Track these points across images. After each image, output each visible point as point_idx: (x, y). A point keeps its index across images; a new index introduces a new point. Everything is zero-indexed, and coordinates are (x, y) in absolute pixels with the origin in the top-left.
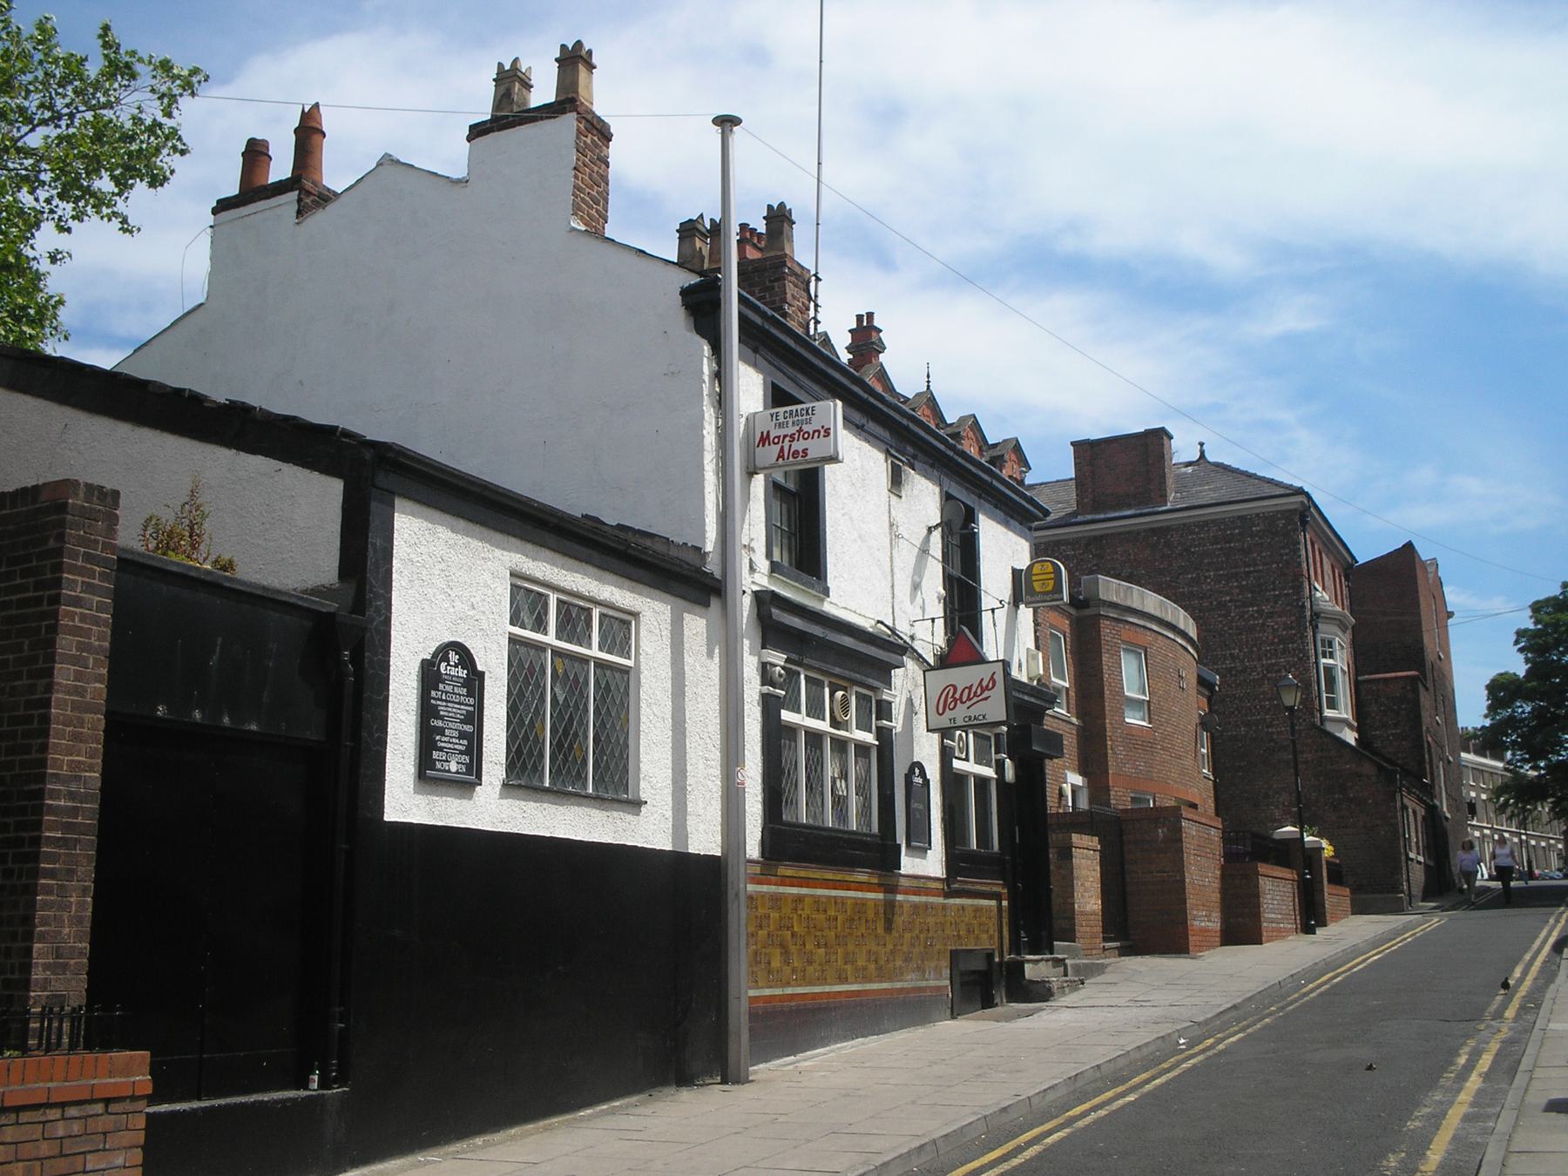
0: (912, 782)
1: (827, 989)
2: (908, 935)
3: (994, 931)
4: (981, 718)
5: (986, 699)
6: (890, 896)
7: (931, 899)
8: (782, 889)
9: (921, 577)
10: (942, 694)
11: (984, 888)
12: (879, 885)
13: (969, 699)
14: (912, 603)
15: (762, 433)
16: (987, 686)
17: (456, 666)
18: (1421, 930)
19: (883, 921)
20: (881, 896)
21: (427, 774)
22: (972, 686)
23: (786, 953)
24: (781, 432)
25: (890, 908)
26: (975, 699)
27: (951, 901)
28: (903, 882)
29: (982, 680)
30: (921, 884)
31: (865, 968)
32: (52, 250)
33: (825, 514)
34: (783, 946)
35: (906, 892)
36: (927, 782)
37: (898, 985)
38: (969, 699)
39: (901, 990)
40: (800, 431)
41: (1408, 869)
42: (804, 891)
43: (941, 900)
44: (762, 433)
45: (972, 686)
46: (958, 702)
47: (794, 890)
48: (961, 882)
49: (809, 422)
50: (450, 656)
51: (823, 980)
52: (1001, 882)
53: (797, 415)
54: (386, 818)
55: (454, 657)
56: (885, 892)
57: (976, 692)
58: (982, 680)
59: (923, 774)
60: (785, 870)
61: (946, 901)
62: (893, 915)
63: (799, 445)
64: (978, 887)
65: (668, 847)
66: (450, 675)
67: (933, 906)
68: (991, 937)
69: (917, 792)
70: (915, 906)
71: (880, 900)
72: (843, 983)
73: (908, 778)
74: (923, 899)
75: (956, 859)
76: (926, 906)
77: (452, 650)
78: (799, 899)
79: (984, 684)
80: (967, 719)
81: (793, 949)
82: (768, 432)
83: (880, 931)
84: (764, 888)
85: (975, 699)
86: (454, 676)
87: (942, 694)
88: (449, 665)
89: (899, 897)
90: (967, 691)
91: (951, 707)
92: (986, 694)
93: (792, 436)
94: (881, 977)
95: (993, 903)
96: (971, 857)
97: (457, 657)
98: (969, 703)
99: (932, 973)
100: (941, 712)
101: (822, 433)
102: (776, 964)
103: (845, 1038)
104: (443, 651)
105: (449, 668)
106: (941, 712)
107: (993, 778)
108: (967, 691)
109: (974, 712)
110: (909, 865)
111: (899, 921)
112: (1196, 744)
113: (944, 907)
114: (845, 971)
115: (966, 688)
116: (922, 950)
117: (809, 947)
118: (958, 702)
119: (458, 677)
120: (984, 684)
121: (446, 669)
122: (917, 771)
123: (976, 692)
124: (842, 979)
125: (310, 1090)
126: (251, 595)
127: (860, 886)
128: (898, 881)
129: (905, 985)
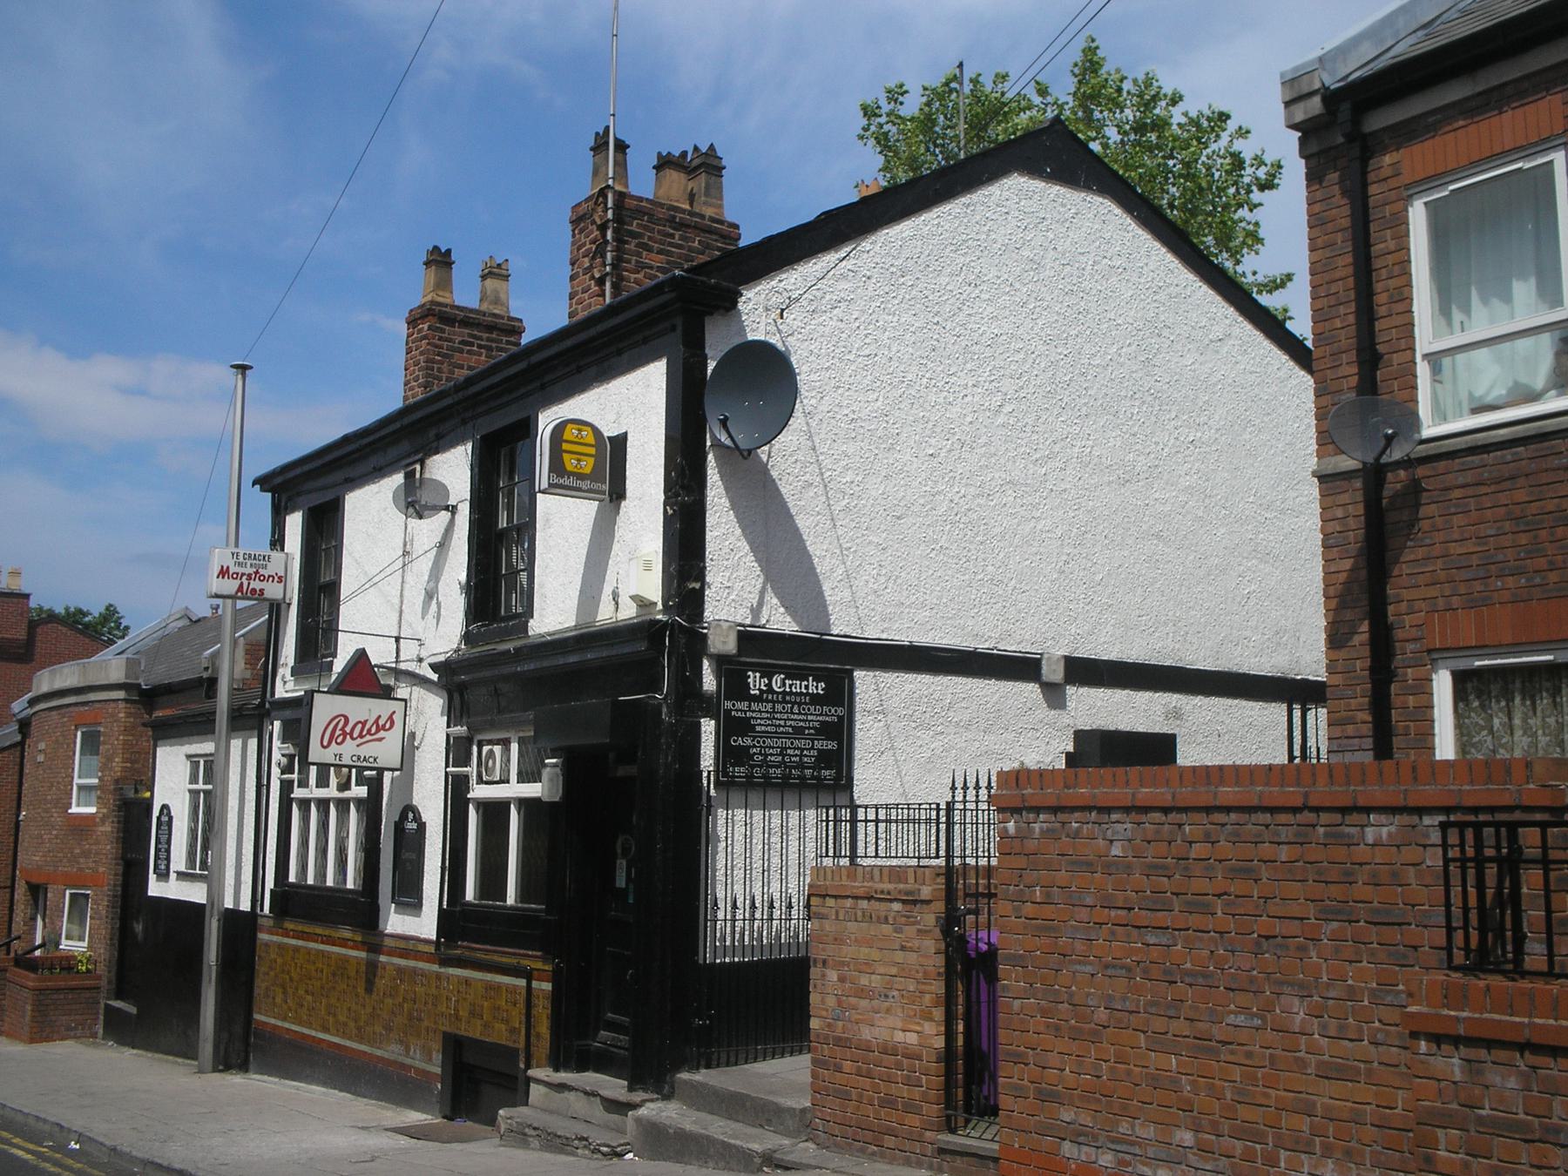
0: (404, 829)
1: (313, 1033)
2: (389, 1001)
3: (520, 1023)
5: (381, 739)
6: (372, 956)
7: (421, 965)
8: (286, 940)
9: (437, 582)
11: (504, 960)
12: (363, 943)
13: (361, 736)
14: (423, 618)
15: (222, 567)
16: (384, 725)
19: (364, 980)
20: (363, 954)
22: (366, 721)
23: (285, 993)
24: (240, 570)
25: (372, 968)
27: (451, 971)
28: (388, 942)
29: (380, 716)
30: (408, 947)
31: (345, 1024)
32: (892, 85)
34: (284, 987)
35: (391, 953)
36: (422, 827)
37: (379, 1053)
38: (361, 736)
39: (381, 1059)
40: (257, 573)
41: (1448, 905)
42: (300, 943)
43: (435, 968)
44: (222, 567)
45: (366, 721)
47: (294, 942)
48: (461, 949)
49: (265, 567)
51: (309, 1025)
52: (539, 954)
53: (255, 559)
54: (150, 893)
56: (368, 951)
57: (369, 730)
58: (380, 716)
59: (417, 818)
60: (289, 925)
61: (442, 970)
62: (375, 976)
63: (256, 585)
64: (496, 958)
65: (231, 907)
67: (423, 974)
68: (513, 1031)
69: (410, 840)
70: (400, 971)
71: (362, 959)
72: (325, 1032)
73: (399, 828)
74: (412, 963)
75: (454, 919)
76: (414, 971)
78: (296, 949)
80: (354, 758)
81: (290, 991)
82: (228, 568)
83: (361, 990)
84: (275, 938)
85: (368, 738)
86: (801, 694)
89: (383, 958)
91: (339, 741)
92: (382, 734)
93: (249, 575)
94: (361, 1040)
95: (522, 982)
96: (470, 912)
98: (359, 741)
99: (418, 1052)
100: (325, 743)
101: (276, 578)
102: (278, 1000)
103: (324, 1084)
106: (325, 743)
108: (360, 726)
109: (365, 751)
110: (396, 923)
111: (381, 983)
112: (1463, 486)
113: (438, 976)
114: (328, 1020)
115: (360, 722)
116: (406, 1022)
117: (301, 992)
120: (381, 722)
121: (784, 685)
122: (411, 815)
123: (369, 730)
124: (326, 1030)
126: (1513, 406)
127: (343, 943)
128: (382, 941)
129: (386, 1055)
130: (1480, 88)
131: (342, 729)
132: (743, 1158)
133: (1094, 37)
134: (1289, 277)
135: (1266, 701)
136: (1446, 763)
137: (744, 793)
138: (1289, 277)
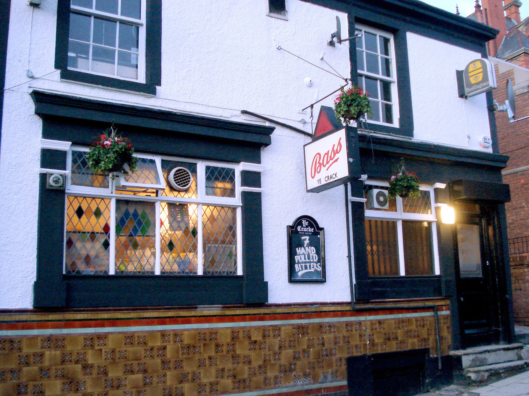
4: (334, 176)
5: (336, 160)
10: (312, 167)
16: (337, 150)
17: (307, 227)
18: (385, 263)
21: (480, 275)
22: (328, 152)
26: (331, 162)
29: (334, 145)
33: (392, 69)
38: (327, 163)
45: (328, 152)
46: (322, 166)
50: (303, 222)
55: (305, 223)
57: (331, 157)
66: (303, 232)
77: (304, 220)
79: (335, 149)
80: (327, 179)
85: (331, 162)
86: (306, 232)
87: (312, 167)
88: (302, 227)
90: (326, 156)
92: (337, 156)
97: (308, 223)
98: (328, 166)
100: (313, 176)
104: (299, 222)
105: (302, 228)
106: (313, 176)
107: (433, 221)
108: (326, 156)
109: (330, 173)
118: (322, 166)
119: (308, 232)
120: (335, 149)
123: (331, 157)
125: (487, 365)
130: (40, 319)
131: (319, 163)
132: (403, 2)
133: (330, 48)
134: (337, 17)
135: (128, 125)
136: (464, 332)
137: (463, 275)
138: (337, 17)
